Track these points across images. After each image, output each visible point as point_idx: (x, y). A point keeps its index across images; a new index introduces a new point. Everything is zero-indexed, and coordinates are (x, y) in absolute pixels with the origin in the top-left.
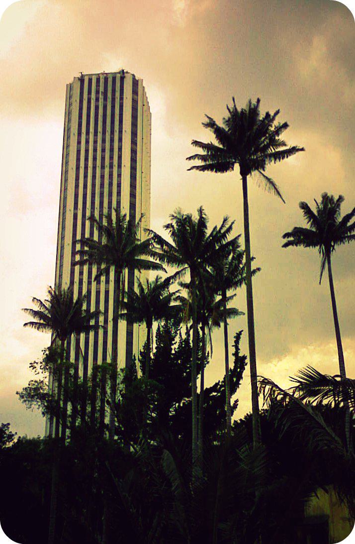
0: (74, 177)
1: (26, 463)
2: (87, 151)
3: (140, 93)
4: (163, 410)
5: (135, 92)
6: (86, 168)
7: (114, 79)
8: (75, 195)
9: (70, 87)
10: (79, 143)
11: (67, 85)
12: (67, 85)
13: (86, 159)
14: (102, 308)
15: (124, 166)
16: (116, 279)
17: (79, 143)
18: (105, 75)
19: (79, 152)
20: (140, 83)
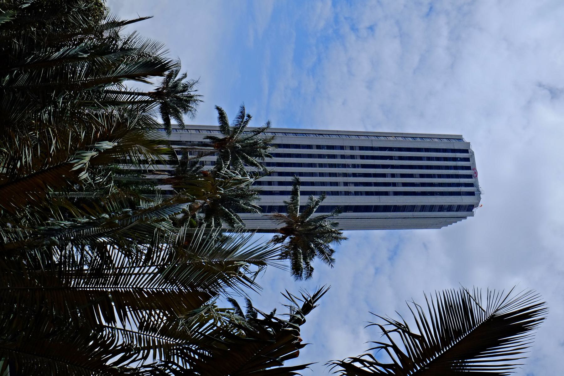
0: (456, 148)
1: (39, 113)
2: (391, 158)
3: (459, 214)
4: (203, 262)
5: (459, 208)
6: (429, 159)
7: (471, 185)
8: (333, 146)
9: (459, 139)
10: (319, 147)
11: (462, 136)
12: (462, 136)
13: (438, 159)
14: (289, 179)
15: (481, 206)
16: (275, 192)
17: (319, 147)
18: (475, 175)
19: (309, 147)
20: (469, 213)
